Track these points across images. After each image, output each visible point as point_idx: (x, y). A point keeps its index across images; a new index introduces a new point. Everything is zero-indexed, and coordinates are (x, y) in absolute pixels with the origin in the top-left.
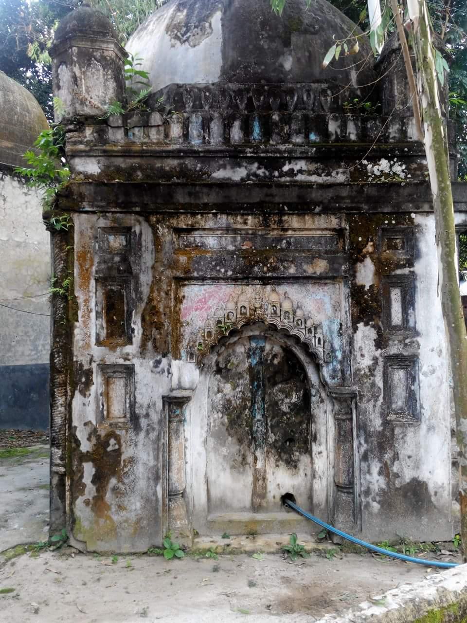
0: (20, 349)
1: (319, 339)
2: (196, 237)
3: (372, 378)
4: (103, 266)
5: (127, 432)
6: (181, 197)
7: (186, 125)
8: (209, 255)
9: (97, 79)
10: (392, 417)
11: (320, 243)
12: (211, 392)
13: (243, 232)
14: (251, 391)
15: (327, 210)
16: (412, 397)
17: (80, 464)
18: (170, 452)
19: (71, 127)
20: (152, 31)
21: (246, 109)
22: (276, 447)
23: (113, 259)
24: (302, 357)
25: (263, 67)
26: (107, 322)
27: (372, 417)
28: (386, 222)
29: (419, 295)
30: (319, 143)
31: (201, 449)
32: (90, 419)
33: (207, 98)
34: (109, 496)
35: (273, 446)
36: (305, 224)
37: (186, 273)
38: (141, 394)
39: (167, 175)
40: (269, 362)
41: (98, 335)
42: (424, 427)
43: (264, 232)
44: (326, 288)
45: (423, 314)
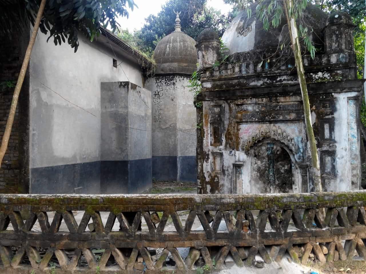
0: (191, 149)
1: (293, 144)
2: (244, 107)
4: (212, 119)
5: (221, 175)
6: (238, 93)
7: (240, 67)
8: (249, 113)
10: (325, 175)
12: (252, 164)
13: (262, 104)
14: (268, 164)
16: (334, 168)
18: (236, 183)
19: (202, 72)
20: (232, 29)
23: (215, 116)
24: (288, 151)
25: (270, 41)
28: (321, 97)
29: (336, 127)
31: (248, 184)
32: (209, 170)
33: (248, 56)
35: (278, 185)
37: (240, 120)
39: (234, 86)
41: (211, 142)
42: (338, 180)
43: (270, 104)
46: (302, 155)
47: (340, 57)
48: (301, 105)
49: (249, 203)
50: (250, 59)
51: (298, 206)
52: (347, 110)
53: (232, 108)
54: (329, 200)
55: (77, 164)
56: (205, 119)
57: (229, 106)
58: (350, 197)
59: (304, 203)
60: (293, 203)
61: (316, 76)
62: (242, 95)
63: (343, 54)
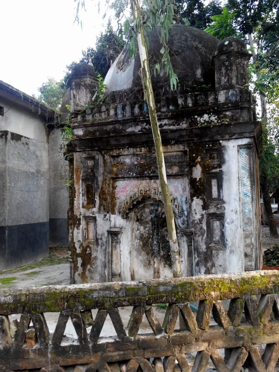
1: (176, 205)
2: (121, 159)
3: (201, 225)
4: (84, 174)
6: (113, 142)
7: (116, 109)
10: (212, 245)
12: (134, 230)
13: (141, 155)
15: (177, 142)
16: (223, 235)
17: (76, 258)
18: (112, 255)
22: (164, 258)
27: (201, 244)
28: (207, 146)
29: (225, 184)
34: (87, 273)
35: (163, 257)
38: (99, 229)
39: (108, 132)
41: (83, 204)
42: (228, 251)
43: (150, 155)
44: (179, 180)
46: (186, 219)
48: (185, 155)
49: (37, 302)
50: (127, 99)
51: (116, 303)
52: (237, 162)
53: (107, 161)
54: (165, 291)
56: (77, 174)
57: (104, 158)
58: (199, 286)
59: (127, 298)
60: (108, 299)
61: (202, 119)
62: (117, 145)
63: (232, 91)
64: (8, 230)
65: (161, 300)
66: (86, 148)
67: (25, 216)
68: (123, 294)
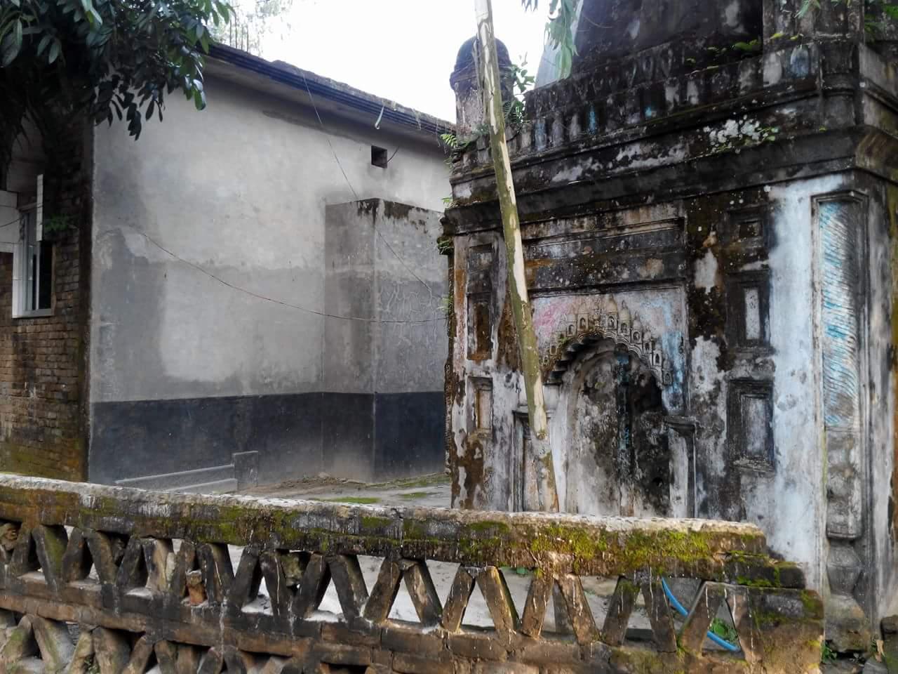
1: (657, 357)
3: (713, 408)
4: (472, 284)
7: (532, 132)
9: (475, 106)
11: (660, 239)
12: (579, 415)
13: (582, 236)
15: (661, 199)
17: (457, 468)
21: (587, 99)
22: (644, 486)
23: (479, 275)
26: (478, 337)
27: (713, 458)
28: (732, 203)
29: (774, 297)
30: (656, 117)
33: (553, 97)
35: (641, 483)
36: (639, 219)
38: (497, 407)
40: (636, 383)
41: (469, 349)
42: (780, 480)
43: (601, 234)
44: (666, 294)
45: (779, 324)
46: (681, 391)
47: (791, 63)
49: (207, 522)
54: (441, 535)
55: (243, 397)
56: (459, 284)
58: (520, 534)
59: (362, 539)
61: (721, 133)
64: (378, 402)
65: (430, 552)
66: (474, 226)
67: (417, 375)
68: (354, 527)
